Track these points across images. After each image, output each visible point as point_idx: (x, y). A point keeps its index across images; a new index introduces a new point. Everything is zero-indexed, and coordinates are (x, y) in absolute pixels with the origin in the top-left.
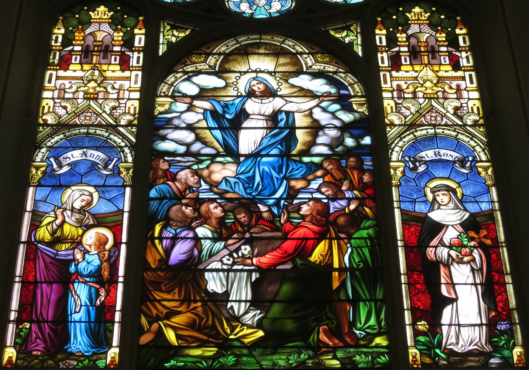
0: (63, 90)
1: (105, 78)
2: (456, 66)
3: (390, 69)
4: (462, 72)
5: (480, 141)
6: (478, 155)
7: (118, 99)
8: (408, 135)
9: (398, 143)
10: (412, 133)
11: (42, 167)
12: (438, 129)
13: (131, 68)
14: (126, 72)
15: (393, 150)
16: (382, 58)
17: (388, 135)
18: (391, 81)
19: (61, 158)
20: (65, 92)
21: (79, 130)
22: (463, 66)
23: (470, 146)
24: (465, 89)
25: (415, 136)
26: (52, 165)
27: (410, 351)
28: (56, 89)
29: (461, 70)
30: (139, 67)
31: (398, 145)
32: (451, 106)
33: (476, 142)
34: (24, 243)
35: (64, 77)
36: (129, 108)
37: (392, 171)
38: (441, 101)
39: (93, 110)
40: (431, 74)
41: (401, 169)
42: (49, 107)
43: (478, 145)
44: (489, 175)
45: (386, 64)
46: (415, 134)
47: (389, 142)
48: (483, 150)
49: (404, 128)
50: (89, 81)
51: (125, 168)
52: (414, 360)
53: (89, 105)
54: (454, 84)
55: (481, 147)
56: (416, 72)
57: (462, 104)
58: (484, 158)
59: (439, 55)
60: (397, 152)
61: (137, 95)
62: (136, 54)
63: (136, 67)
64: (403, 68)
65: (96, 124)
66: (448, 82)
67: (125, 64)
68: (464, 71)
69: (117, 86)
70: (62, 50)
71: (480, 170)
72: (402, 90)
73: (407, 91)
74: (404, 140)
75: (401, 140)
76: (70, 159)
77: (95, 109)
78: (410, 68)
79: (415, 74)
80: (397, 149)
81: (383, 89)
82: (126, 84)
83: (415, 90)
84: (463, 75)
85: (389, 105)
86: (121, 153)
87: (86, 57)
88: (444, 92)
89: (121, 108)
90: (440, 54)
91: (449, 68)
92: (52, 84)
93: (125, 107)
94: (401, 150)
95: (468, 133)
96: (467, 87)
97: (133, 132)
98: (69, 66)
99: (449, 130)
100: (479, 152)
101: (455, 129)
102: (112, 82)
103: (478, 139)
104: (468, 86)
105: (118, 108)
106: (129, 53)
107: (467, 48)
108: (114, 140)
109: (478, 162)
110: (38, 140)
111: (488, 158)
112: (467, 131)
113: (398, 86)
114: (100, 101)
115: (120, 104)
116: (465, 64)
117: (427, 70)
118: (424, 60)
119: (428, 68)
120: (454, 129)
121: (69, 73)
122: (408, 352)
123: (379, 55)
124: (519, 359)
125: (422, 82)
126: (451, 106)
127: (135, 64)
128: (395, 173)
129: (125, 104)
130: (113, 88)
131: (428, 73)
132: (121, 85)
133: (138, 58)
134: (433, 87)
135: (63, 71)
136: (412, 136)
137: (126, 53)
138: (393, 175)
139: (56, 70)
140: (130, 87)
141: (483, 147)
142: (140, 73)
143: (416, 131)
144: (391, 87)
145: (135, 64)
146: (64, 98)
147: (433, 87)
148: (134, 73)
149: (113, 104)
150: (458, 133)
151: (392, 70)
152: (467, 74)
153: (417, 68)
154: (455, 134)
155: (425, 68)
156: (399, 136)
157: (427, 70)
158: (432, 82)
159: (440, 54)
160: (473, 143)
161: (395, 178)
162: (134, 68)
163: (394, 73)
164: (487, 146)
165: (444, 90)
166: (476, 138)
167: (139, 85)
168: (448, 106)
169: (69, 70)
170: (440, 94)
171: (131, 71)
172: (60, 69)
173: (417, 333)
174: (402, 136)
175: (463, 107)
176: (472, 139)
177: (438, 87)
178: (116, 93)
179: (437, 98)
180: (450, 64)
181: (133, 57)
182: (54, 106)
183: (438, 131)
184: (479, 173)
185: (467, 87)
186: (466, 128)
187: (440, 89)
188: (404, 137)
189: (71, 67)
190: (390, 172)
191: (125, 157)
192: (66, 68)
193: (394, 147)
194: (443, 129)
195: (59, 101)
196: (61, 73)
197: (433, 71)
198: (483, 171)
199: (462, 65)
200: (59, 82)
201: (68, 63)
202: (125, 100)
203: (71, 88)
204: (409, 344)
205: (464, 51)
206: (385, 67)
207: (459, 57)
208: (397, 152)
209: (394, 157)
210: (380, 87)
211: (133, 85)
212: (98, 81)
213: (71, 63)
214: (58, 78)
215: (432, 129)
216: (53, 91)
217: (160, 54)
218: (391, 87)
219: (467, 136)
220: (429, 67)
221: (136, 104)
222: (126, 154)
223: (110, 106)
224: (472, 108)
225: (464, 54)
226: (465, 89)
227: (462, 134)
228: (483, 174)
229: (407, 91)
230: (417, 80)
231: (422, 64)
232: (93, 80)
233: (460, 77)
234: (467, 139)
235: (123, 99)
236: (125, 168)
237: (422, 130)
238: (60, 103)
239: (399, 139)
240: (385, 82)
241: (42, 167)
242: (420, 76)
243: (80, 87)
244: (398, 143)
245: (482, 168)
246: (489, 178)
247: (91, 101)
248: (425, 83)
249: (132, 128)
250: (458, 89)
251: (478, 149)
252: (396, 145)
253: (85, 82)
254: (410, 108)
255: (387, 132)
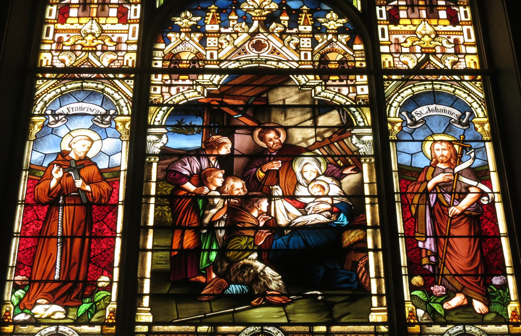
0: (398, 43)
1: (103, 31)
2: (453, 19)
3: (388, 22)
4: (460, 27)
5: (476, 97)
6: (476, 111)
7: (116, 51)
8: (406, 90)
9: (396, 98)
10: (410, 88)
11: (397, 122)
12: (436, 84)
13: (129, 21)
14: (457, 26)
15: (391, 106)
16: (381, 12)
17: (385, 91)
18: (389, 34)
19: (413, 113)
20: (63, 45)
21: (98, 84)
22: (461, 21)
23: (468, 102)
24: (463, 44)
25: (413, 91)
26: (406, 120)
27: (406, 305)
28: (55, 42)
29: (459, 25)
30: (136, 19)
31: (396, 100)
32: (449, 60)
33: (473, 98)
34: (153, 196)
35: (62, 30)
36: (127, 61)
37: (389, 126)
38: (439, 56)
39: (434, 65)
40: (429, 29)
41: (399, 125)
42: (47, 61)
43: (476, 101)
44: (126, 129)
45: (385, 17)
46: (414, 89)
47: (386, 98)
48: (480, 107)
49: (402, 83)
50: (87, 34)
51: (121, 122)
52: (410, 314)
53: (88, 58)
54: (453, 37)
55: (478, 103)
56: (81, 24)
57: (459, 58)
58: (481, 115)
59: (90, 7)
60: (395, 107)
61: (135, 47)
62: (133, 7)
63: (134, 20)
64: (401, 22)
65: (94, 78)
66: (110, 35)
67: (122, 17)
68: (462, 25)
69: (115, 39)
70: (59, 3)
71: (477, 126)
72: (399, 44)
73: (66, 43)
74: (402, 95)
75: (399, 95)
76: (415, 113)
77: (436, 65)
78: (408, 22)
79: (414, 28)
80: (395, 104)
81: (380, 42)
82: (124, 37)
83: (412, 44)
84: (461, 30)
85: (386, 59)
86: (117, 107)
87: (84, 9)
88: (442, 47)
89: (461, 63)
90: (109, 6)
91: (447, 22)
92: (51, 37)
93: (123, 60)
94: (399, 106)
95: (465, 89)
96: (464, 42)
97: (129, 85)
98: (66, 19)
99: (446, 85)
100: (476, 108)
101: (452, 84)
102: (110, 35)
103: (474, 95)
104: (465, 41)
105: (117, 61)
106: (127, 6)
107: (466, 3)
108: (108, 92)
109: (118, 116)
110: (386, 95)
111: (484, 115)
112: (461, 85)
113: (397, 39)
114: (99, 54)
115: (118, 56)
116: (463, 19)
117: (425, 24)
118: (93, 12)
119: (426, 22)
120: (450, 85)
121: (65, 26)
122: (404, 307)
123: (378, 9)
124: (514, 314)
125: (420, 36)
126: (449, 60)
127: (132, 17)
128: (393, 128)
129: (124, 56)
130: (111, 41)
131: (423, 28)
132: (119, 38)
133: (135, 10)
134: (431, 41)
135: (60, 24)
136: (410, 91)
137: (124, 5)
138: (391, 130)
139: (54, 24)
140: (128, 40)
141: (480, 104)
142: (137, 26)
143: (414, 86)
144: (389, 41)
145: (463, 19)
146: (401, 53)
147: (431, 41)
148: (132, 26)
149: (453, 58)
150: (456, 89)
151: (390, 24)
152: (465, 28)
153: (416, 22)
154: (453, 89)
155: (423, 22)
156: (397, 92)
157: (425, 24)
158: (430, 37)
159: (437, 8)
160: (469, 99)
161: (32, 132)
162: (132, 21)
163: (392, 27)
164: (484, 102)
165: (104, 43)
166: (472, 94)
167: (136, 38)
168: (446, 61)
169: (66, 23)
170: (438, 49)
171: (129, 24)
172: (57, 23)
173: (412, 288)
174: (400, 92)
175: (460, 62)
176: (469, 95)
177: (435, 41)
178: (452, 47)
179: (96, 50)
180: (447, 19)
181: (130, 9)
182: (52, 59)
183: (435, 86)
184: (476, 129)
185: (464, 42)
186: (114, 82)
187: (438, 43)
188: (402, 92)
189: (69, 20)
190: (387, 127)
191: (121, 110)
192: (63, 22)
193: (393, 102)
194: (441, 85)
195: (398, 55)
196: (59, 26)
197: (431, 25)
198: (479, 127)
199: (460, 20)
200: (394, 37)
201: (66, 16)
202: (124, 53)
203: (406, 42)
204: (406, 299)
205: (461, 5)
206: (384, 21)
207: (128, 9)
208: (395, 107)
209: (392, 114)
210: (378, 41)
211: (131, 38)
212: (431, 35)
213: (69, 17)
214: (390, 32)
215: (430, 84)
216: (51, 44)
217: (157, 7)
218: (389, 41)
219: (465, 93)
220: (96, 20)
221: (134, 56)
222: (122, 107)
223: (450, 61)
224: (127, 61)
225: (462, 9)
226: (463, 44)
227: (460, 90)
228: (480, 130)
229: (66, 43)
230: (415, 34)
231: (90, 17)
232: (426, 34)
233: (76, 30)
234: (112, 92)
235: (121, 51)
236: (121, 122)
237: (420, 85)
238: (58, 56)
239: (397, 94)
240: (383, 36)
241: (397, 122)
242: (418, 30)
243: (415, 42)
244: (396, 98)
245: (479, 124)
246: (125, 132)
247: (90, 53)
248: (423, 37)
249: (128, 82)
250: (456, 43)
251: (475, 105)
252: (394, 100)
253: (83, 35)
254: (407, 63)
255: (385, 88)
